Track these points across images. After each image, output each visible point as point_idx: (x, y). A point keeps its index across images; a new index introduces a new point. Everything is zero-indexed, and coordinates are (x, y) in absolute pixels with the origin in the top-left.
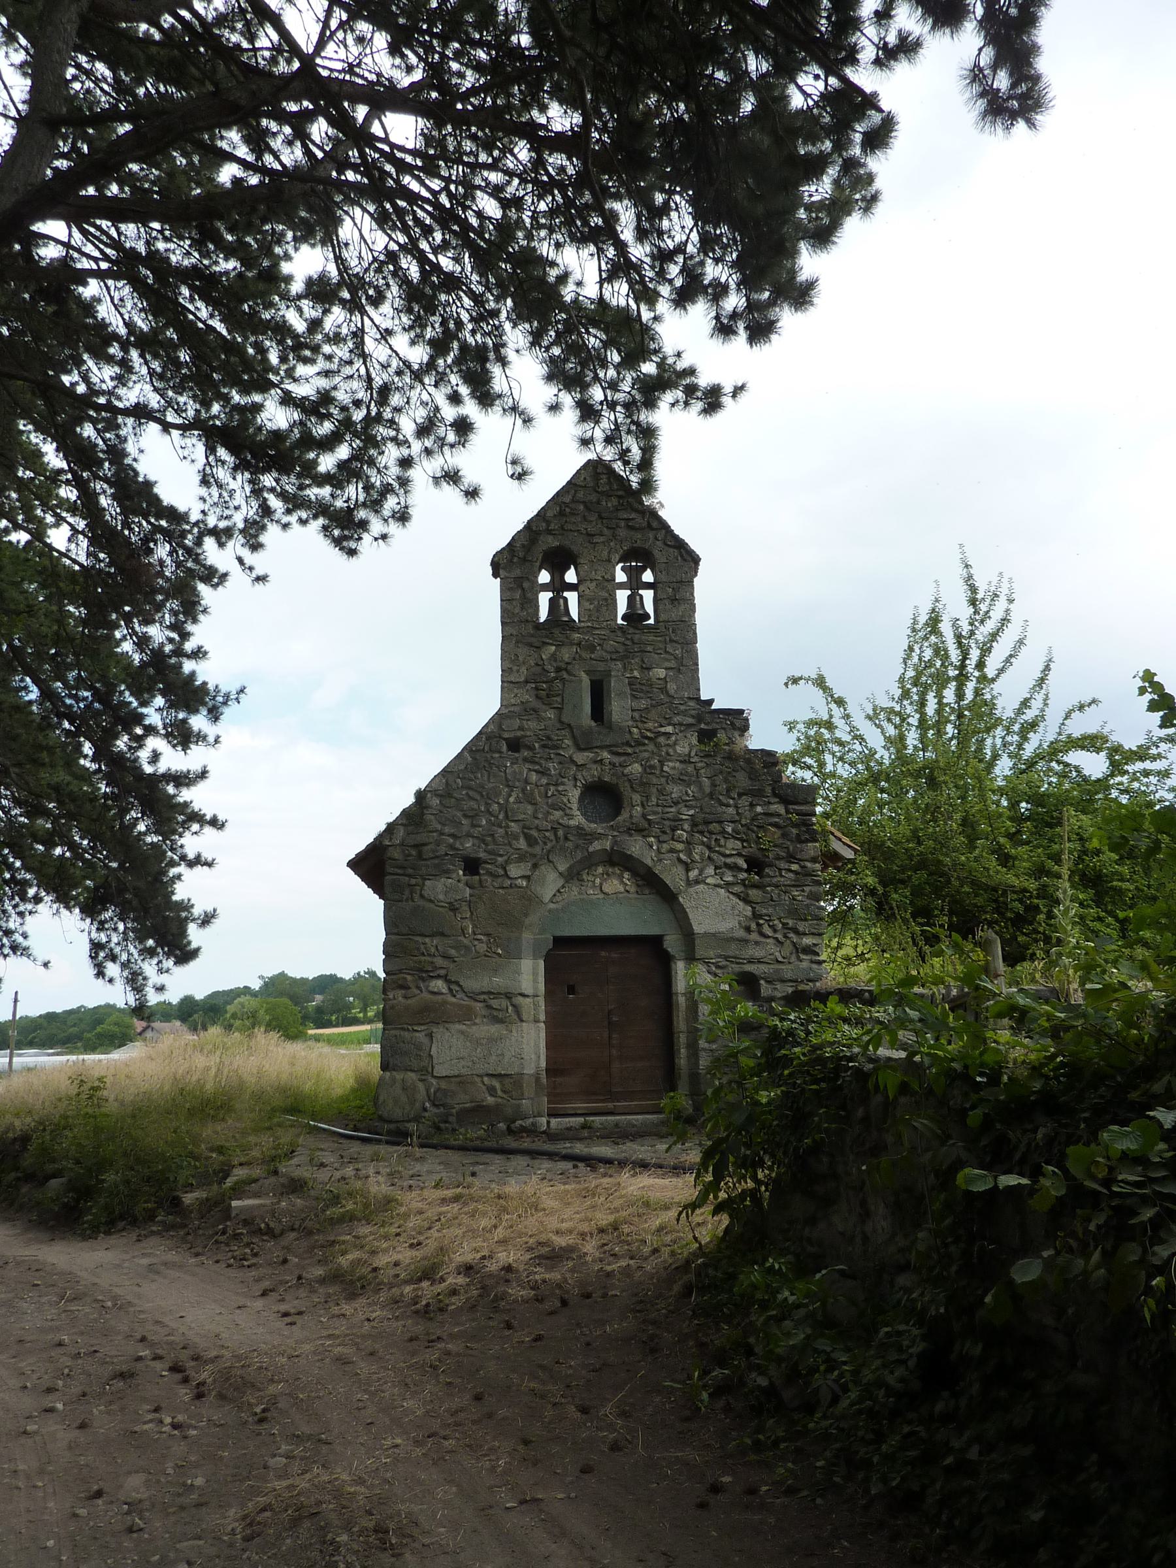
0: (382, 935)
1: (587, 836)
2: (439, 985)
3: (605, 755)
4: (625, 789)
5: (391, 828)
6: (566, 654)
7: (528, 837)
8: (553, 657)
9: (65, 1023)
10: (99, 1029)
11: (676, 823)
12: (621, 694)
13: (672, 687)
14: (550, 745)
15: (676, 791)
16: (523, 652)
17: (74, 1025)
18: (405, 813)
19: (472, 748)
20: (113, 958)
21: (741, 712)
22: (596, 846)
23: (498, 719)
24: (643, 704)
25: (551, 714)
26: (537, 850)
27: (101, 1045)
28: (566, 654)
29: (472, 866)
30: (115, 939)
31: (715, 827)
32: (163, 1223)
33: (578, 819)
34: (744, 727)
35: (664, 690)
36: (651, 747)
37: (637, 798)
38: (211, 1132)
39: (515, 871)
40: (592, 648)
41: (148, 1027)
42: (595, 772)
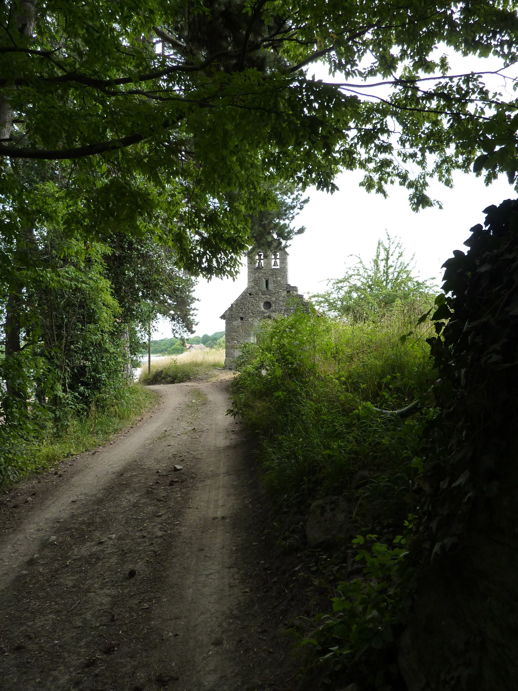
0: (468, 238)
1: (264, 313)
2: (236, 342)
3: (268, 296)
4: (272, 303)
5: (226, 311)
6: (260, 275)
7: (252, 313)
8: (258, 276)
9: (160, 344)
10: (173, 347)
11: (281, 310)
12: (271, 284)
13: (281, 282)
14: (257, 294)
15: (281, 303)
16: (252, 275)
17: (164, 345)
18: (229, 308)
19: (242, 295)
20: (177, 332)
21: (295, 287)
22: (265, 315)
23: (247, 289)
24: (276, 285)
25: (257, 288)
26: (254, 315)
27: (174, 353)
28: (260, 275)
29: (242, 319)
30: (177, 328)
31: (289, 311)
32: (76, 45)
33: (263, 309)
34: (296, 291)
35: (280, 282)
36: (277, 294)
37: (274, 305)
38: (198, 369)
39: (250, 320)
40: (265, 274)
41: (191, 346)
42: (266, 300)
